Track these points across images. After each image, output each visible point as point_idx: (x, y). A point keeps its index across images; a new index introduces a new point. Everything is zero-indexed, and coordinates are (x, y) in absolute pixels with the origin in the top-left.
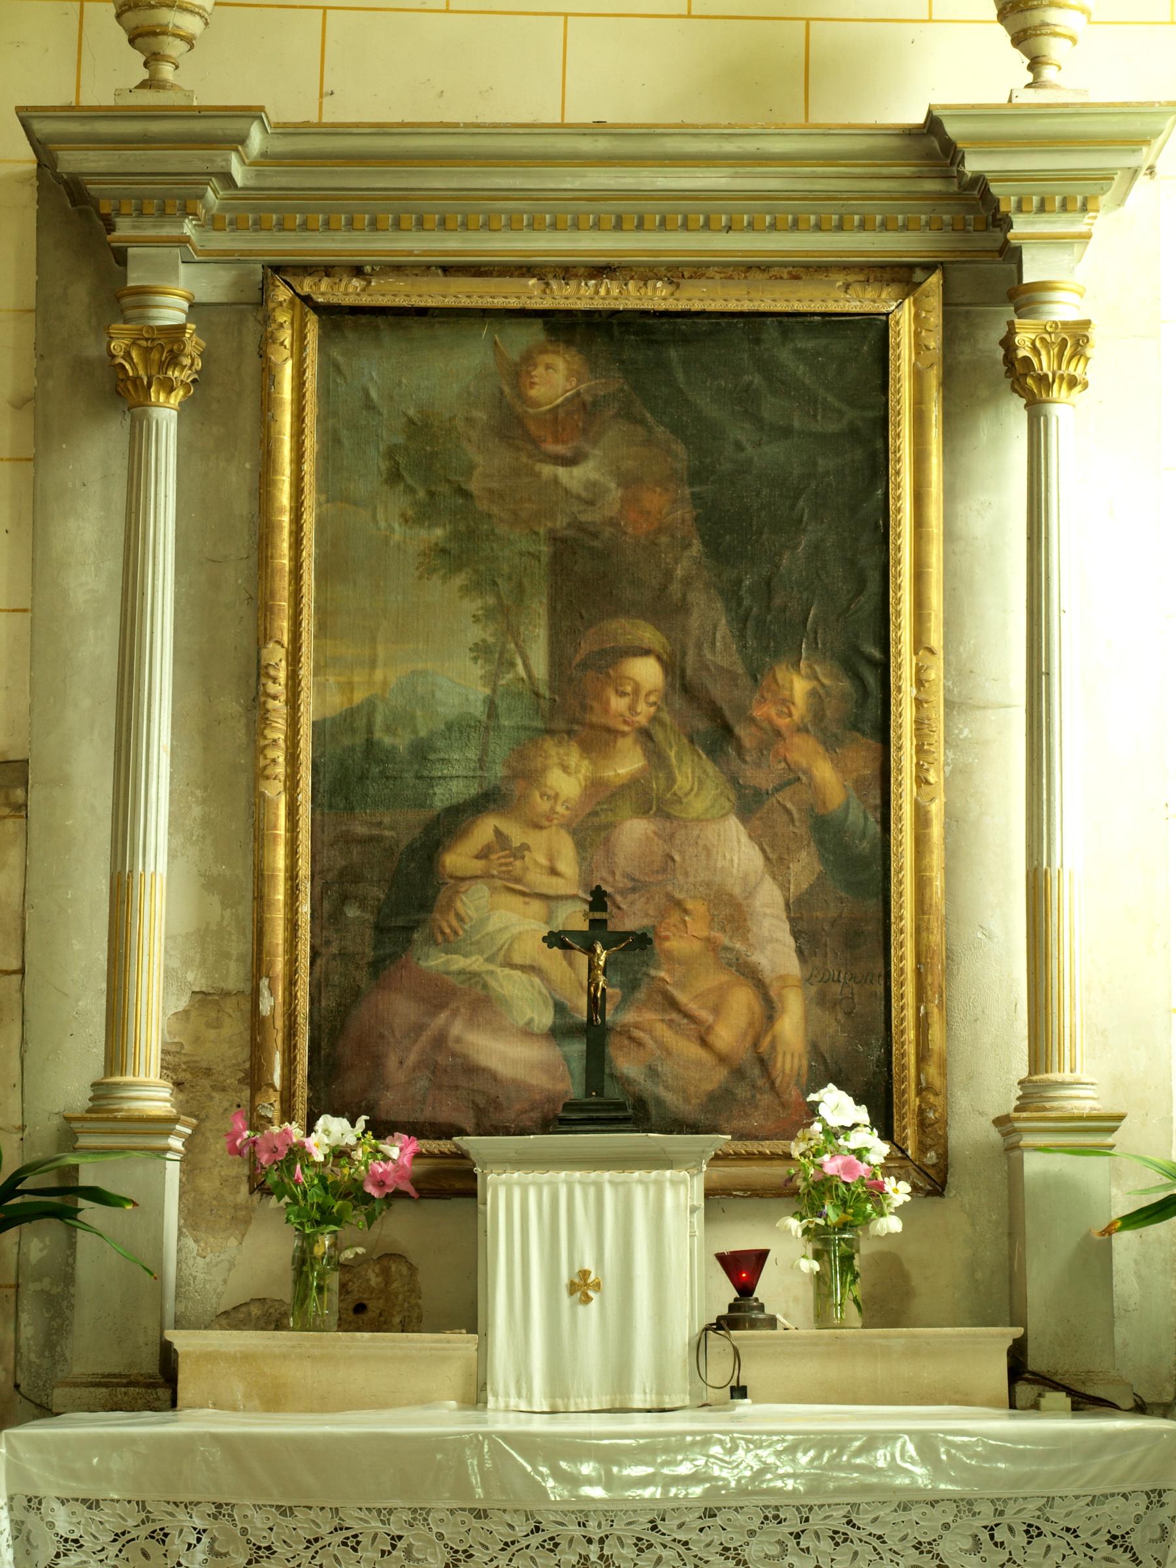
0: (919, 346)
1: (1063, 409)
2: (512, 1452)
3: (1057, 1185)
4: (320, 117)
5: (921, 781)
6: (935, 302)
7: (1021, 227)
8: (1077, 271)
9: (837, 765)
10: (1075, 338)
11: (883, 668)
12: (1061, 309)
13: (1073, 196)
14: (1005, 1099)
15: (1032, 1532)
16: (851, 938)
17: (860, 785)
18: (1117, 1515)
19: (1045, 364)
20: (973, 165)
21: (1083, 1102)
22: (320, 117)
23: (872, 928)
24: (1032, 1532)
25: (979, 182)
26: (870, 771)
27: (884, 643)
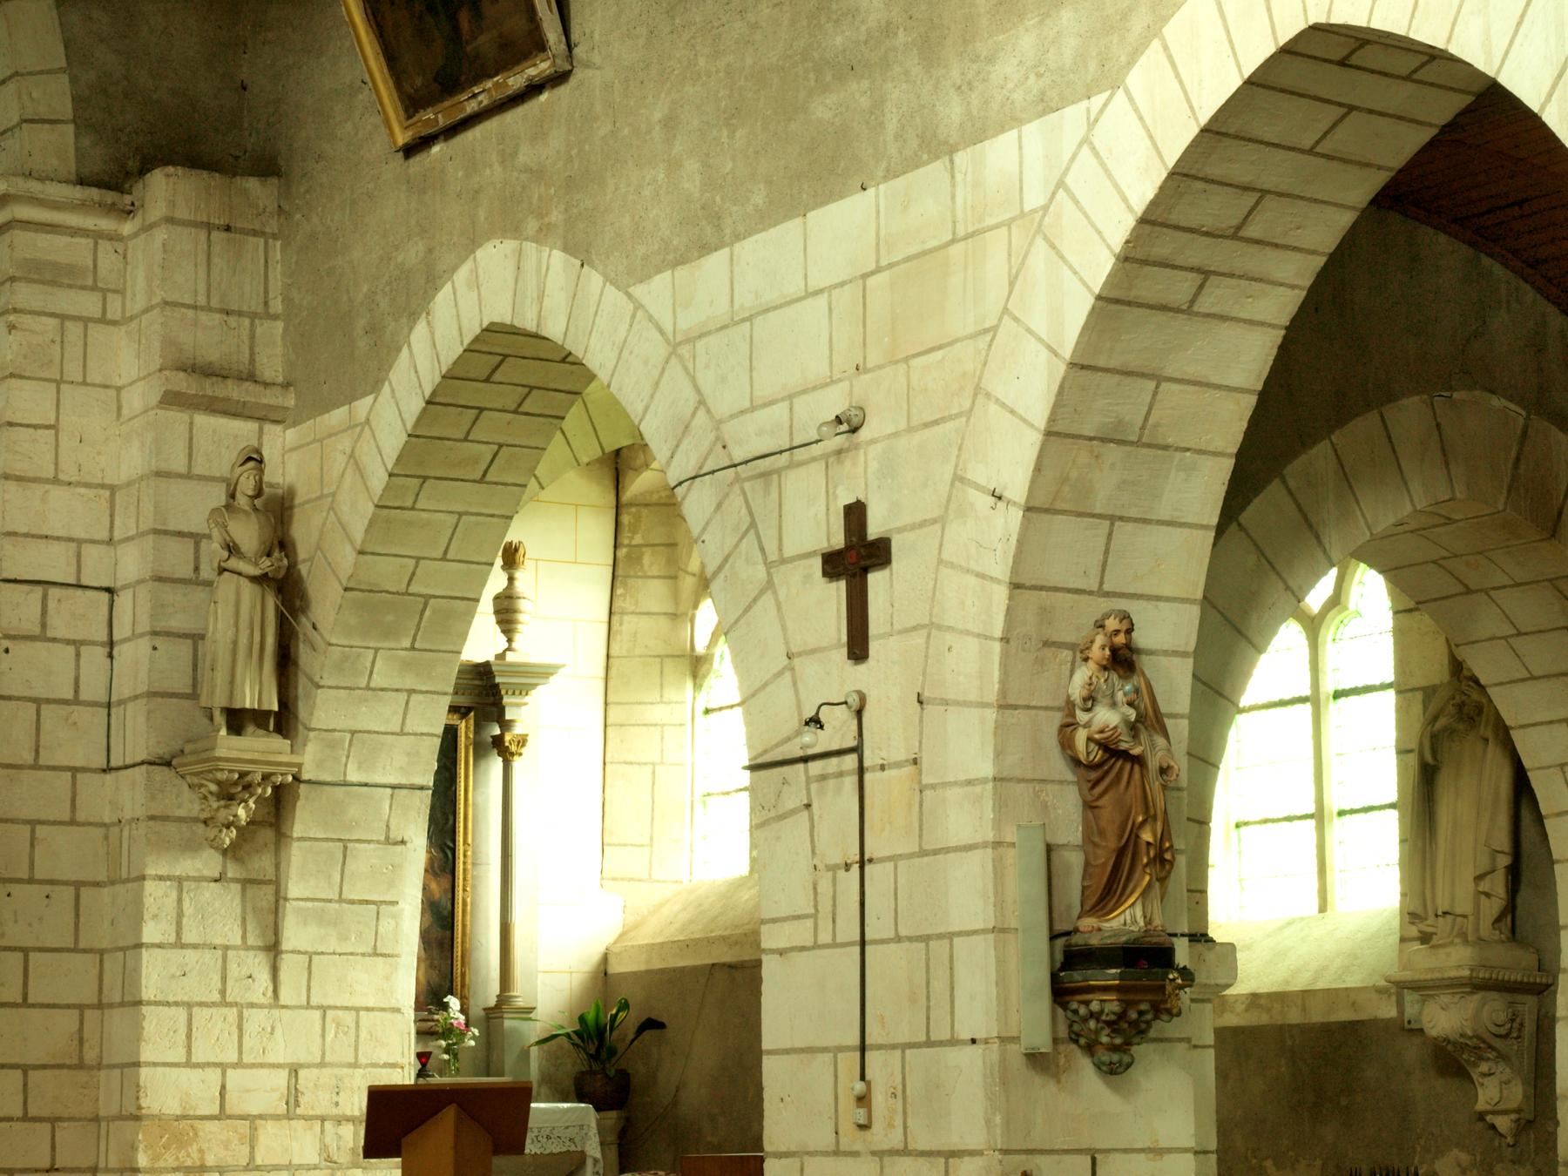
0: (467, 737)
1: (517, 764)
2: (566, 1105)
3: (514, 1031)
4: (770, 1052)
5: (464, 890)
6: (472, 722)
7: (506, 700)
8: (525, 714)
9: (438, 883)
10: (522, 741)
11: (454, 851)
12: (518, 730)
13: (523, 690)
14: (492, 1002)
15: (548, 1138)
16: (441, 944)
17: (445, 891)
18: (572, 1132)
19: (513, 748)
20: (498, 680)
21: (520, 1002)
22: (770, 1052)
23: (447, 941)
24: (548, 1138)
25: (497, 685)
26: (448, 886)
27: (454, 841)
